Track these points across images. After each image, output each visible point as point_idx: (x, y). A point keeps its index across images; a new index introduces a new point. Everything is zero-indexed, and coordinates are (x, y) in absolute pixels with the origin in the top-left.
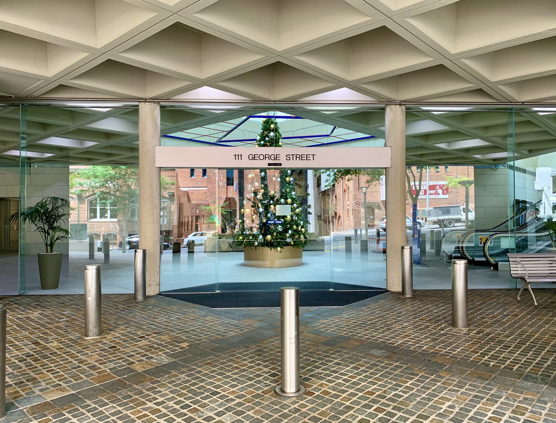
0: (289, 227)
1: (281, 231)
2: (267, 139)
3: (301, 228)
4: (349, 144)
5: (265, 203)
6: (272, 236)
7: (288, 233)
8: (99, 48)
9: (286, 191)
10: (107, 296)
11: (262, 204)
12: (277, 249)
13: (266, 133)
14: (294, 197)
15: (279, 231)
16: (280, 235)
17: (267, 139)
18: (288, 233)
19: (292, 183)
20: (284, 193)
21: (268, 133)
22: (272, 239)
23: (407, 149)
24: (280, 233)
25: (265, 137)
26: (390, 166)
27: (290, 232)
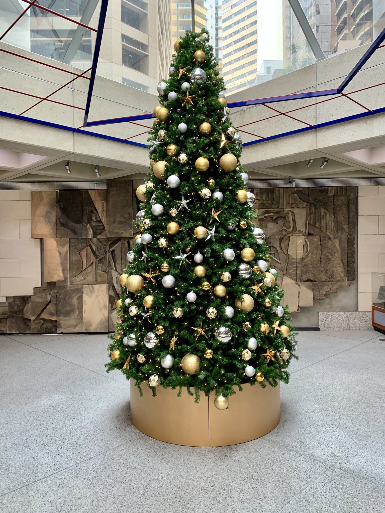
0: (250, 330)
1: (228, 344)
2: (185, 85)
3: (279, 325)
4: (369, 122)
5: (178, 261)
6: (202, 359)
7: (246, 347)
8: (232, 309)
9: (238, 226)
10: (279, 190)
11: (174, 264)
12: (216, 401)
13: (182, 71)
14: (260, 242)
15: (222, 344)
16: (224, 355)
17: (185, 85)
18: (246, 347)
19: (251, 205)
20: (233, 231)
21: (189, 71)
22: (201, 368)
23: (371, 185)
24: (225, 348)
25: (179, 82)
26: (32, 294)
27: (252, 343)
